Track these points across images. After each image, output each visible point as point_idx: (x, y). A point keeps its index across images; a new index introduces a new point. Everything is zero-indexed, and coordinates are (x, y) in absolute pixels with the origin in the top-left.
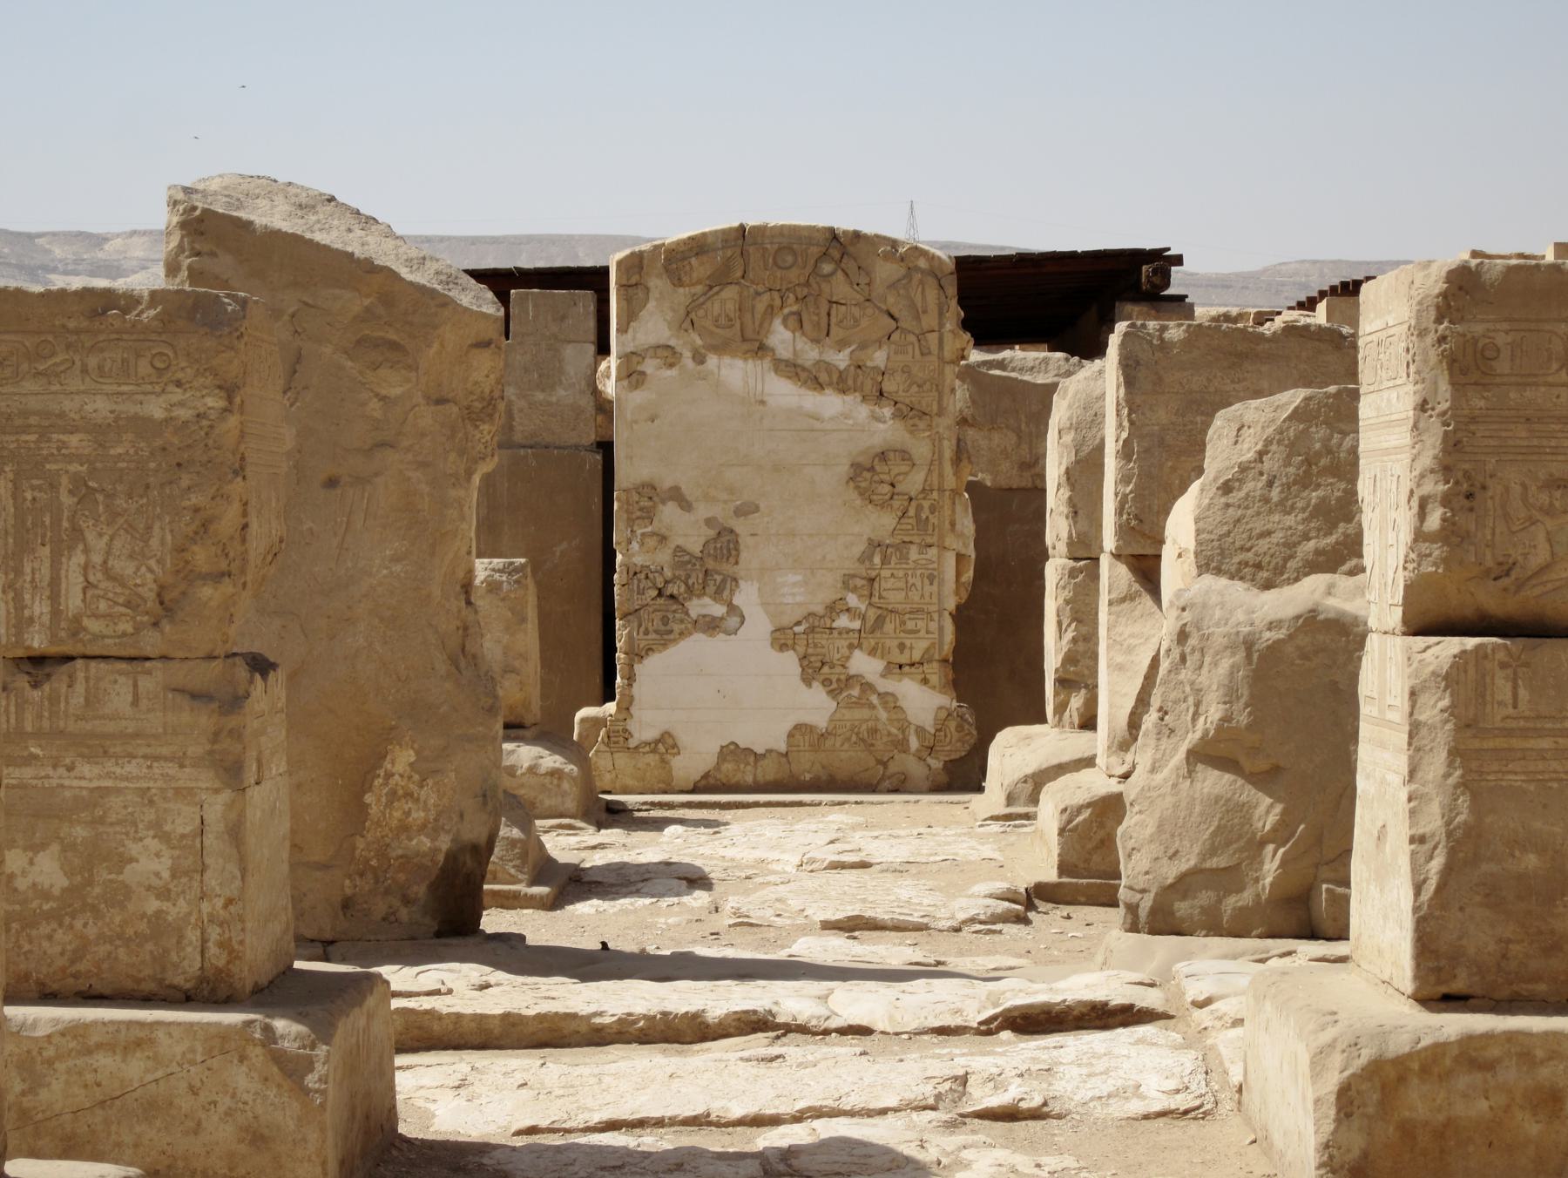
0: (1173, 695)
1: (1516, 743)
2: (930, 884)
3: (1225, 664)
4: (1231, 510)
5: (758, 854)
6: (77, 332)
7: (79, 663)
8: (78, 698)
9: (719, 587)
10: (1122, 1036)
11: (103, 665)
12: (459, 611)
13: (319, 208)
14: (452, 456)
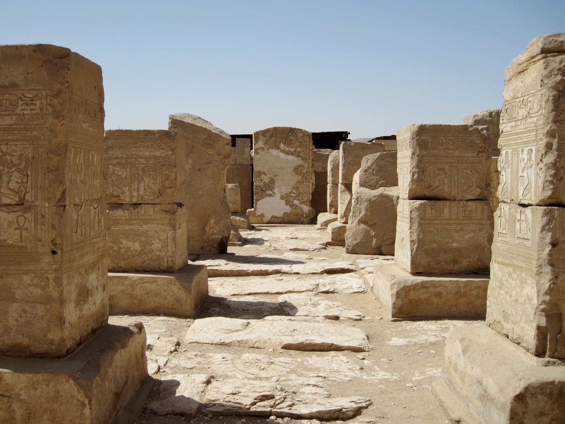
1: (432, 222)
2: (309, 242)
3: (366, 204)
5: (278, 236)
6: (143, 139)
7: (143, 205)
8: (143, 212)
10: (347, 275)
11: (148, 205)
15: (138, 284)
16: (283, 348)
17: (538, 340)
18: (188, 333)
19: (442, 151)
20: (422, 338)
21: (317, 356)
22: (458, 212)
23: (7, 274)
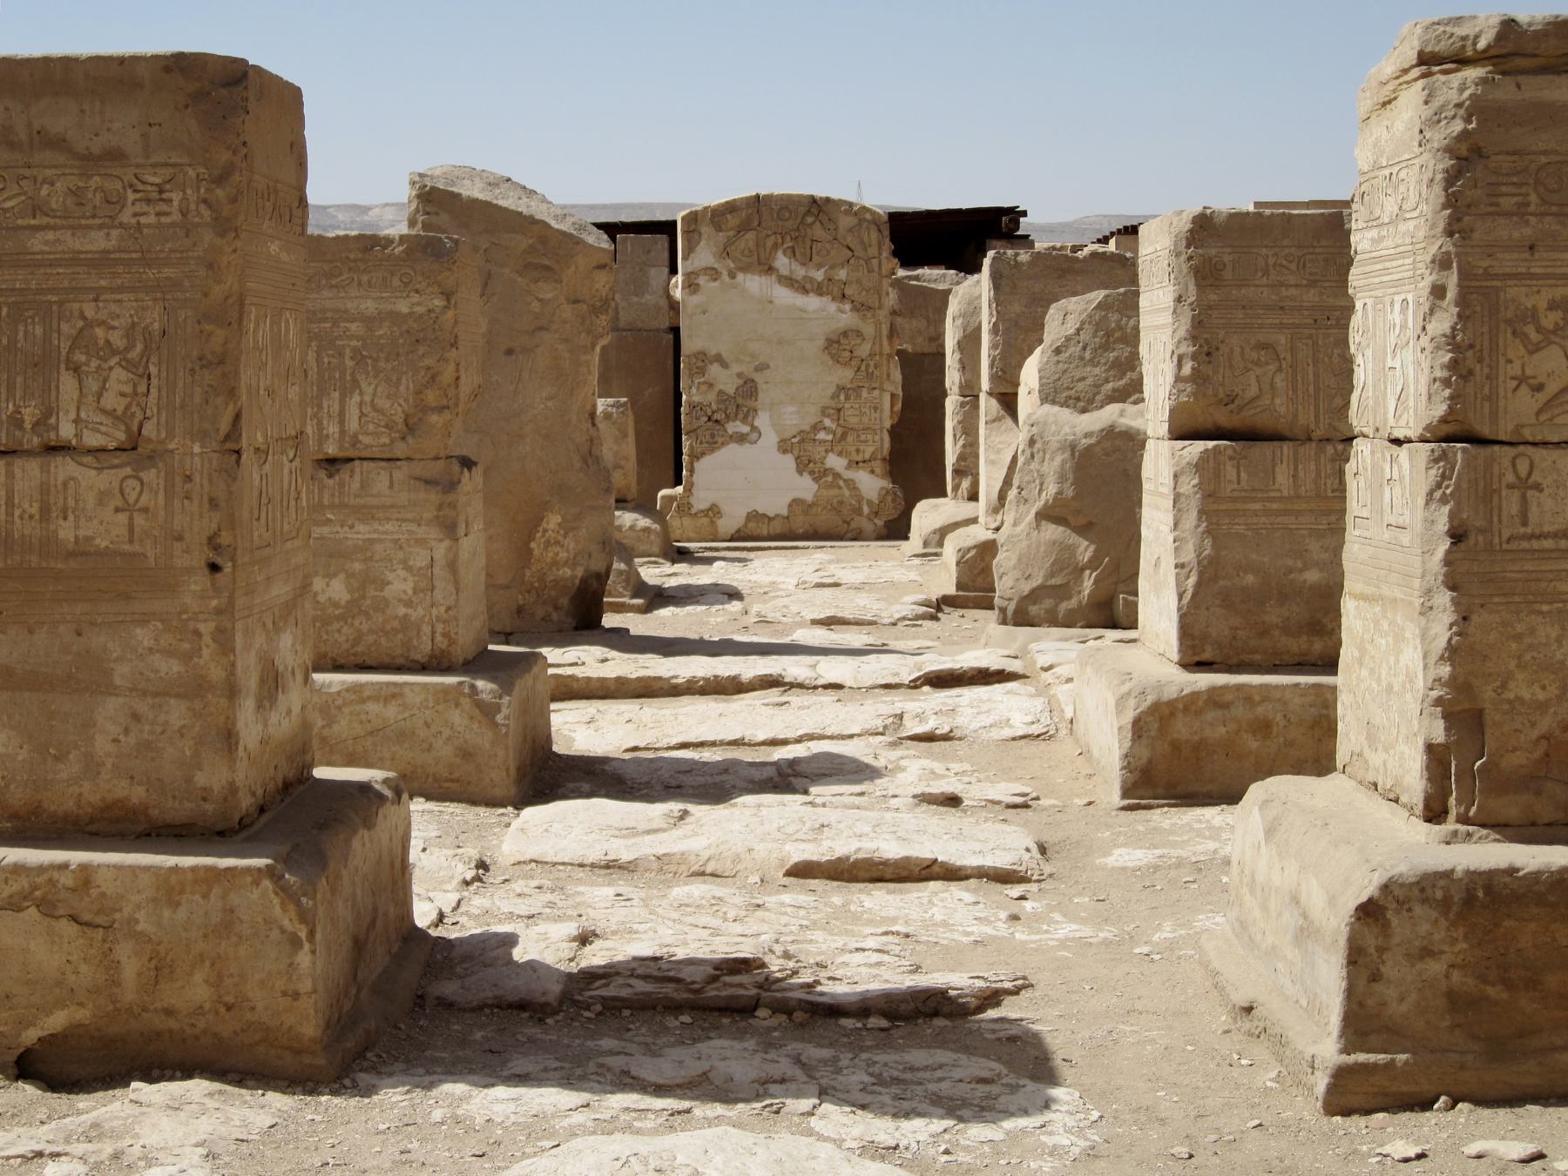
1: (1239, 506)
2: (877, 596)
3: (1059, 459)
6: (355, 261)
7: (357, 463)
8: (356, 485)
10: (998, 688)
11: (372, 464)
15: (345, 704)
16: (789, 873)
17: (1429, 779)
19: (1265, 289)
20: (1200, 848)
21: (889, 892)
22: (1318, 474)
23: (93, 624)
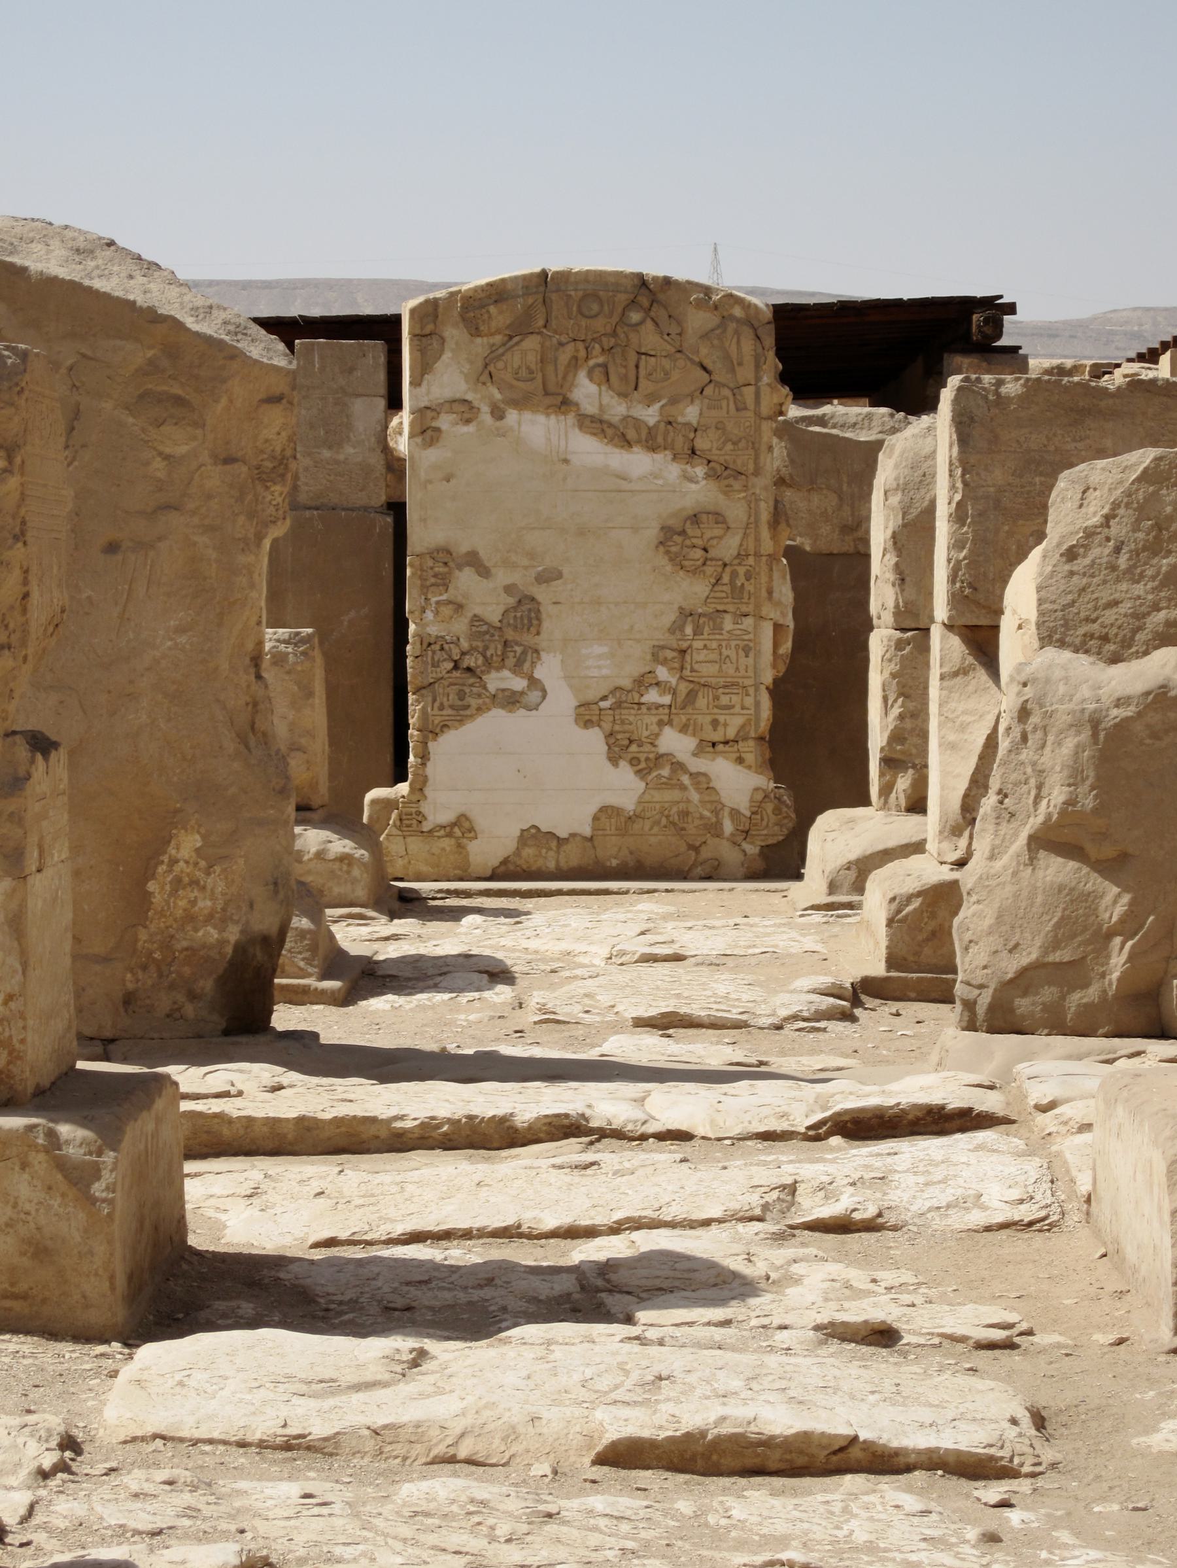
0: (1014, 777)
2: (750, 978)
3: (1070, 743)
4: (1075, 578)
5: (564, 946)
9: (518, 660)
10: (961, 1142)
12: (248, 686)
13: (98, 253)
14: (241, 519)
16: (602, 1460)
18: (112, 1396)
